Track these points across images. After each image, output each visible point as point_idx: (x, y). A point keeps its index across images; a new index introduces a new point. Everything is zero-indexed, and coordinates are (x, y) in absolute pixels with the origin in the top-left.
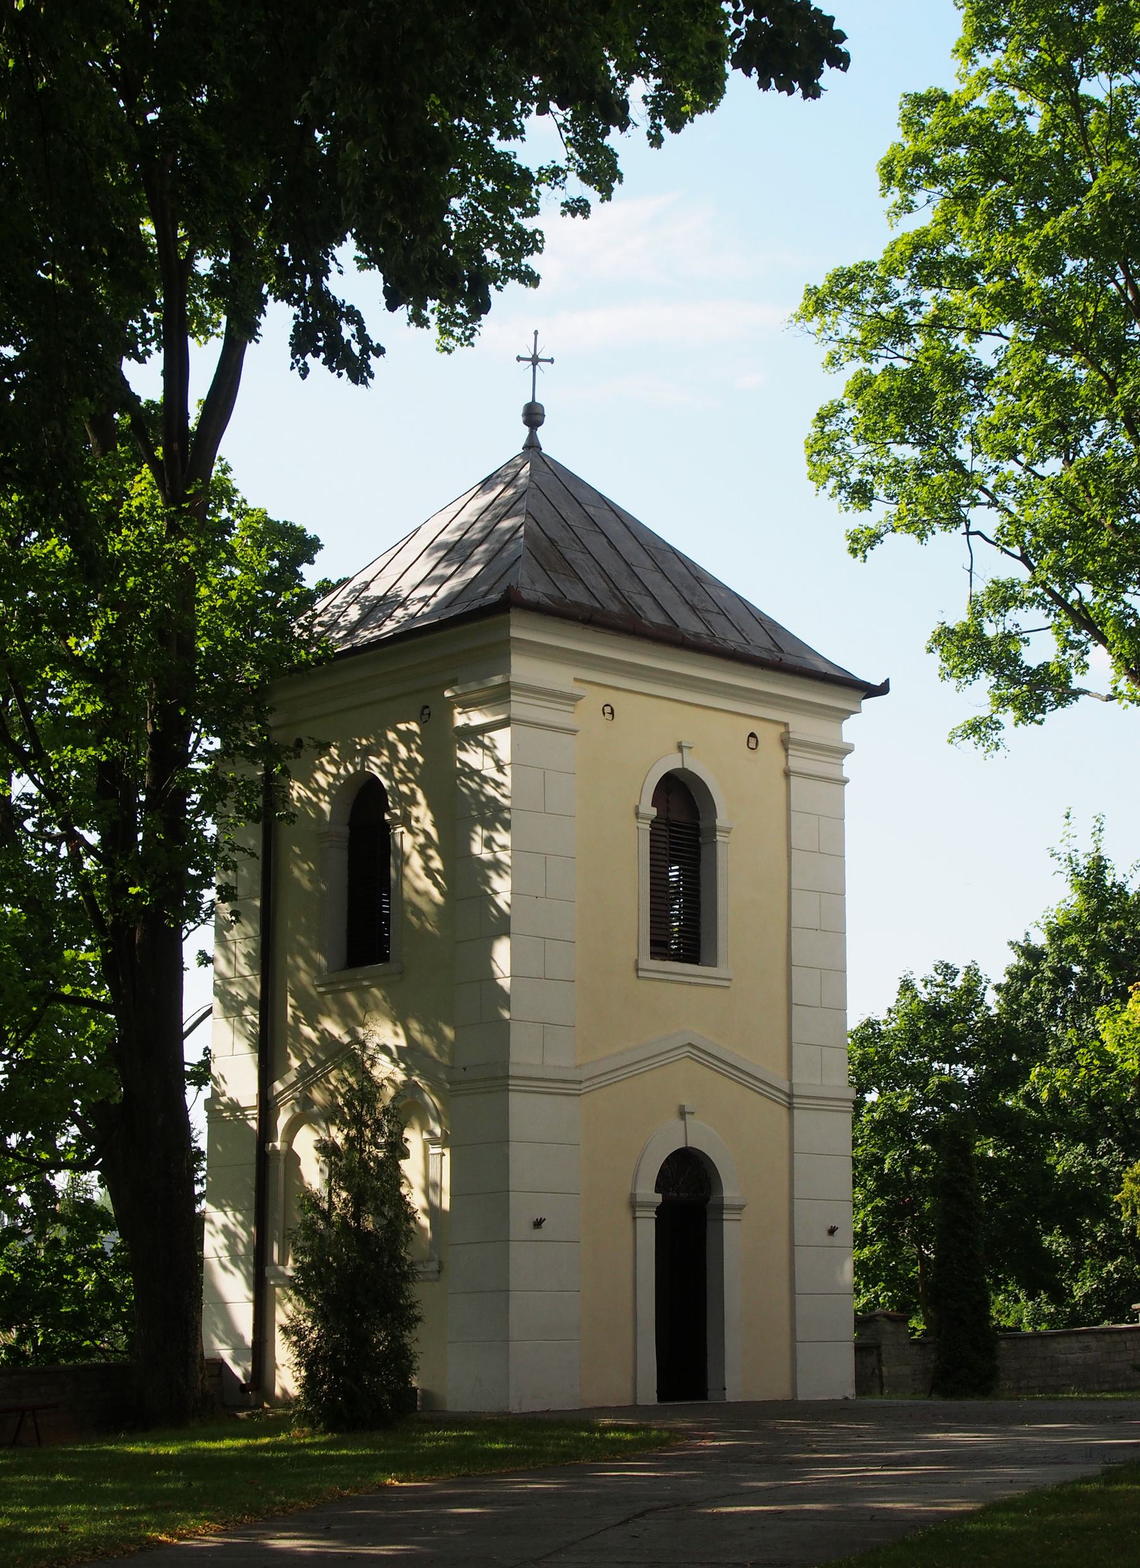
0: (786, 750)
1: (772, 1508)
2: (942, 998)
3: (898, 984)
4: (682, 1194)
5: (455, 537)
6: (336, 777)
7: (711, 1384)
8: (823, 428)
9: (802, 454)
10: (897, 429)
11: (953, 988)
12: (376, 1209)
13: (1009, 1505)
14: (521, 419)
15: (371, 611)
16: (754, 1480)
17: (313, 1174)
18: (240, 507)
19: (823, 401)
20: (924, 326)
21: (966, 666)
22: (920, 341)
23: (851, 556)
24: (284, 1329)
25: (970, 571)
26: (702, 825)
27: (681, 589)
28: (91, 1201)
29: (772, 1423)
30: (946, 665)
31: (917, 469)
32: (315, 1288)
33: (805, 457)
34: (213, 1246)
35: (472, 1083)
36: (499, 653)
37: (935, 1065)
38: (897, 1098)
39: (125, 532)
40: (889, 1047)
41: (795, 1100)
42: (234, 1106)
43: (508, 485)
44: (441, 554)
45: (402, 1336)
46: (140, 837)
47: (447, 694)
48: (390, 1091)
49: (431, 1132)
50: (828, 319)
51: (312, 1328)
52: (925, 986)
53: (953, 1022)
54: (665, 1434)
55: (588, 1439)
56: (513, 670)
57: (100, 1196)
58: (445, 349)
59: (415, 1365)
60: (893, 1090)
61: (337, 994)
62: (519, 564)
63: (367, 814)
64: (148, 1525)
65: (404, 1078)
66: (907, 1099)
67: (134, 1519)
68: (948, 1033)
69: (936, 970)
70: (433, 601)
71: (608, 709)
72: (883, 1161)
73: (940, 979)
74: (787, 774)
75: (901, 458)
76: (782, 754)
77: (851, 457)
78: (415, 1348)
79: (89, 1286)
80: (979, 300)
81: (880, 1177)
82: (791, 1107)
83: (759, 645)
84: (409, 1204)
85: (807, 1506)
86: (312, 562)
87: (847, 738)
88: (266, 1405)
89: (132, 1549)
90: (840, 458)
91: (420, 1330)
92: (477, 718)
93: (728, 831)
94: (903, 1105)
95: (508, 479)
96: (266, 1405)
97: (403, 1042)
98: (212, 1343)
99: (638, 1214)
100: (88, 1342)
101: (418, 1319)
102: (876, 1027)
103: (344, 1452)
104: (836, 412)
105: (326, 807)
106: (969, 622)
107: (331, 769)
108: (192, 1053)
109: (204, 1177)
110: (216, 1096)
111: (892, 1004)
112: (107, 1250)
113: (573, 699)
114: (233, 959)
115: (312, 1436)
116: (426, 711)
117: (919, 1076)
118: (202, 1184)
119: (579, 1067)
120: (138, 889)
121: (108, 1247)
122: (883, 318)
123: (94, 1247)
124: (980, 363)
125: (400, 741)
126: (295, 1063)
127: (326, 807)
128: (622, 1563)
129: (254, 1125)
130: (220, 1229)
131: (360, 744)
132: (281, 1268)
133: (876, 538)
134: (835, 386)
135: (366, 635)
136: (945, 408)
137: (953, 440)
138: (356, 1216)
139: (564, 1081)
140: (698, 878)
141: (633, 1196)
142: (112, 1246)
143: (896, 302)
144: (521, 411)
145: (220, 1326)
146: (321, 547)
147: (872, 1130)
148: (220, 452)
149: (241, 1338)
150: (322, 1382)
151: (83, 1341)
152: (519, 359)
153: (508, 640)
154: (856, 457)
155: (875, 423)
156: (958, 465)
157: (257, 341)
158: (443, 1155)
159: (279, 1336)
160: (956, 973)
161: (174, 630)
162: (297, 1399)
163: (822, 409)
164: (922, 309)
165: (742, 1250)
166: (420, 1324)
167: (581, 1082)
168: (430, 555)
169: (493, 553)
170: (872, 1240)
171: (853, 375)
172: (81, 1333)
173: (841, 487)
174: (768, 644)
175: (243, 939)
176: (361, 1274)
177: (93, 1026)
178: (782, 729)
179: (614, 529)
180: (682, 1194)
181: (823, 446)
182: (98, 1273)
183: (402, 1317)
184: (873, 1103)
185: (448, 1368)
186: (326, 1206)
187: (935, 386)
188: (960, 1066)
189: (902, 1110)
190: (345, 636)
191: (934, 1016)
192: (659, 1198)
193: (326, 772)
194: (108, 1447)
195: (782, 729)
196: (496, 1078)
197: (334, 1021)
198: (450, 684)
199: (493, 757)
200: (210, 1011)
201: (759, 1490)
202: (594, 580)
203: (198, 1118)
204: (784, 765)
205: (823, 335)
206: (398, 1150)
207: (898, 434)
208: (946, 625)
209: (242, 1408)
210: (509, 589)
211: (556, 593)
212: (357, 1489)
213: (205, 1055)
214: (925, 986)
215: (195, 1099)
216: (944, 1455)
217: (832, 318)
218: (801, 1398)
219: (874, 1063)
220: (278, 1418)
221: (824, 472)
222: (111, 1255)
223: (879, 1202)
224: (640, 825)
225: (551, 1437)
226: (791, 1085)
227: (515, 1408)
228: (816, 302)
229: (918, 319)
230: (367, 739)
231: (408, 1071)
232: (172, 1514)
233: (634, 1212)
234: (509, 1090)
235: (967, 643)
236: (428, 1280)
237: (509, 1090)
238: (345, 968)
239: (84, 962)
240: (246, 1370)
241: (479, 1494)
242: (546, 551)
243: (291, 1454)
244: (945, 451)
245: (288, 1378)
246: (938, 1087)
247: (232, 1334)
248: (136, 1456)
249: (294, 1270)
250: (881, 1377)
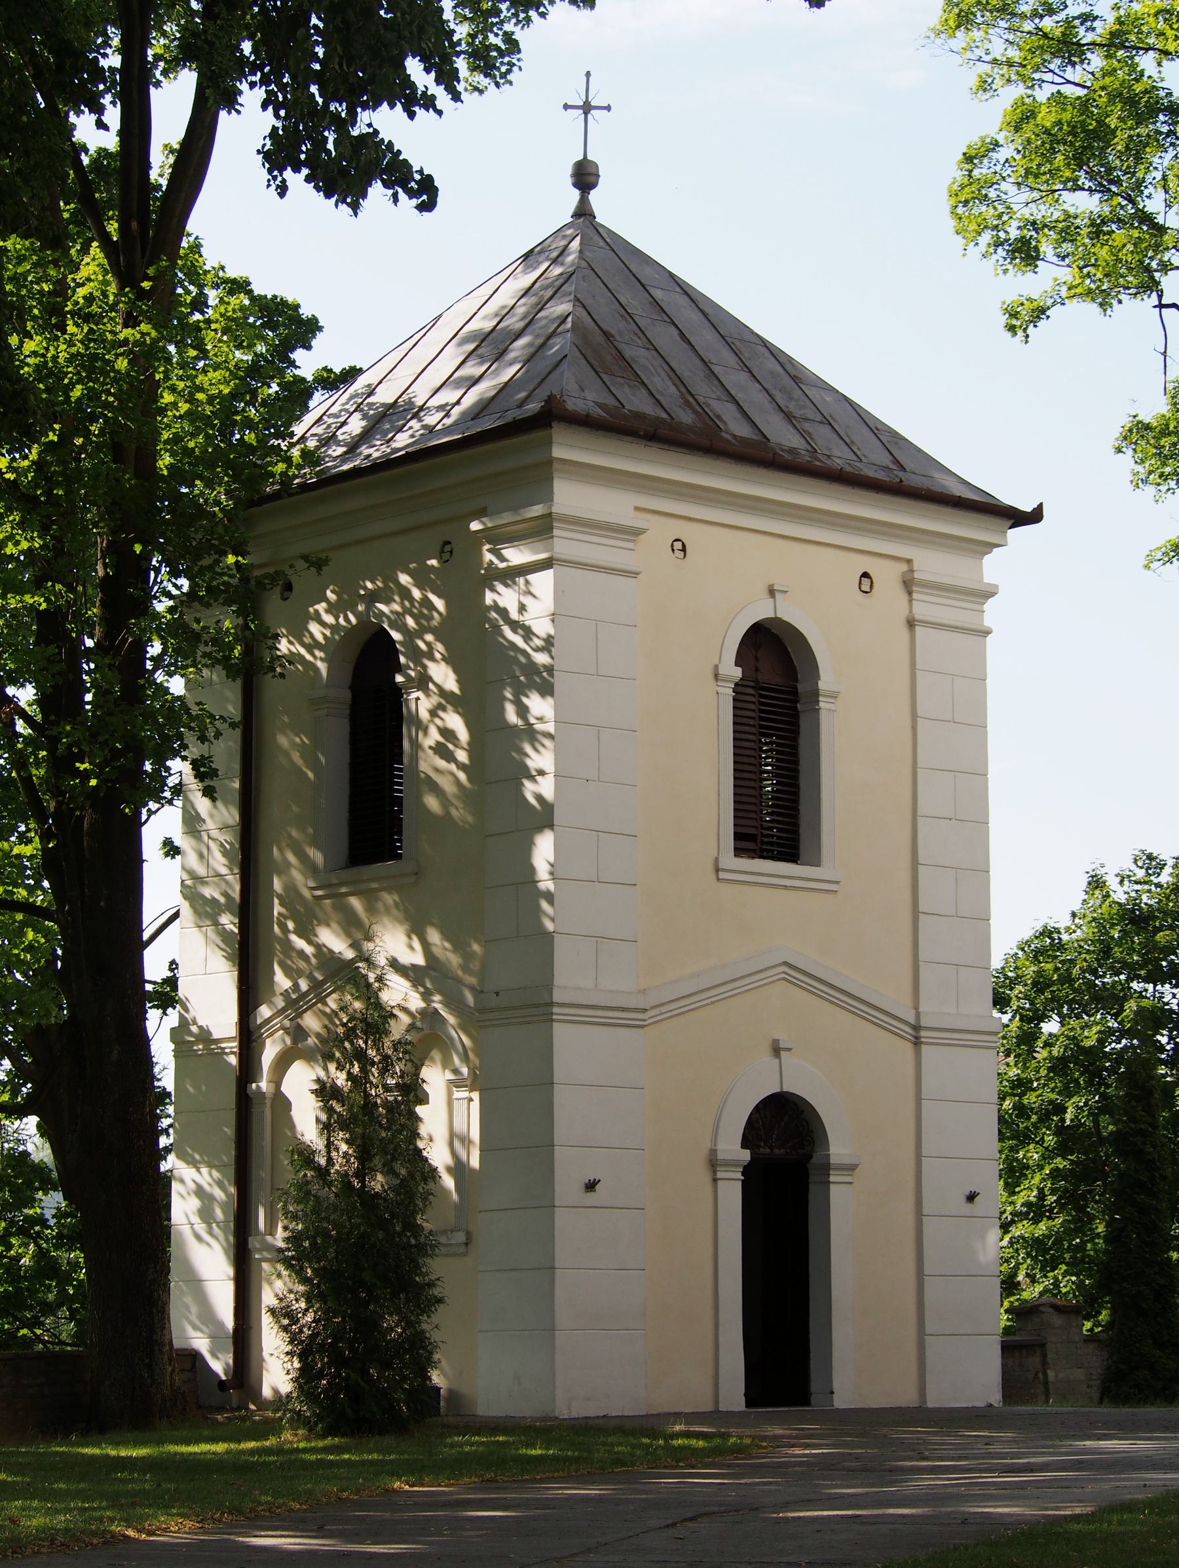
0: (910, 593)
1: (850, 1512)
2: (1144, 898)
3: (1083, 881)
4: (776, 1151)
5: (488, 325)
6: (335, 628)
7: (815, 1385)
8: (971, 171)
9: (945, 204)
10: (1068, 174)
11: (1158, 885)
12: (384, 1165)
13: (1130, 1507)
14: (569, 181)
15: (378, 422)
16: (841, 1487)
17: (306, 1118)
18: (217, 276)
19: (970, 137)
20: (1099, 45)
21: (1167, 470)
22: (1096, 61)
23: (1009, 334)
24: (272, 1311)
25: (1164, 354)
26: (801, 688)
27: (773, 392)
28: (26, 1154)
29: (885, 1430)
30: (1139, 468)
31: (1092, 225)
32: (310, 1262)
33: (947, 209)
34: (183, 1209)
35: (509, 1007)
36: (540, 477)
37: (1135, 985)
38: (1082, 1028)
39: (71, 329)
40: (1072, 962)
41: (923, 1033)
42: (205, 1036)
43: (555, 261)
44: (472, 346)
45: (419, 1323)
46: (88, 697)
47: (475, 526)
48: (405, 1019)
49: (456, 1071)
50: (977, 34)
51: (307, 1310)
52: (1121, 882)
53: (1158, 930)
54: (748, 1441)
55: (648, 1446)
56: (556, 499)
57: (39, 1150)
58: (476, 89)
59: (436, 1357)
60: (1078, 1017)
61: (339, 900)
62: (564, 365)
63: (373, 672)
64: (112, 1520)
65: (422, 1005)
66: (1095, 1029)
67: (97, 1514)
68: (1150, 946)
69: (1135, 861)
70: (456, 412)
71: (678, 545)
72: (1064, 1110)
73: (1140, 874)
74: (911, 624)
75: (1072, 211)
76: (904, 598)
77: (1008, 208)
78: (435, 1336)
79: (25, 1261)
80: (1165, 20)
81: (1060, 1130)
82: (917, 1042)
83: (874, 462)
84: (426, 1160)
85: (891, 1511)
86: (308, 347)
87: (987, 579)
88: (252, 1407)
89: (95, 1542)
90: (995, 208)
91: (441, 1315)
92: (516, 556)
93: (834, 696)
94: (1090, 1038)
95: (555, 254)
96: (252, 1407)
97: (419, 959)
98: (183, 1330)
99: (719, 1175)
100: (25, 1331)
101: (440, 1301)
102: (1055, 936)
103: (347, 1456)
104: (988, 151)
105: (322, 667)
106: (1168, 415)
107: (329, 619)
108: (154, 968)
109: (170, 1126)
110: (184, 1023)
111: (1076, 906)
112: (48, 1215)
113: (636, 532)
114: (205, 852)
115: (308, 1440)
116: (448, 548)
117: (1112, 1000)
118: (168, 1135)
119: (643, 992)
120: (86, 765)
121: (49, 1214)
122: (1045, 36)
123: (31, 1212)
124: (1170, 94)
125: (416, 585)
126: (282, 981)
127: (322, 667)
128: (658, 1562)
129: (233, 1060)
130: (192, 1191)
131: (365, 588)
132: (269, 1238)
133: (1040, 313)
134: (989, 117)
135: (375, 451)
136: (1127, 148)
137: (1139, 185)
138: (360, 1174)
139: (624, 1009)
140: (795, 755)
141: (713, 1152)
142: (54, 1211)
143: (1062, 16)
144: (569, 170)
145: (194, 1309)
146: (320, 329)
147: (1050, 1069)
148: (191, 226)
149: (221, 1325)
150: (320, 1375)
151: (18, 1329)
152: (566, 107)
153: (550, 462)
154: (1015, 207)
155: (1039, 166)
156: (1146, 218)
157: (238, 112)
158: (471, 1100)
159: (266, 1319)
160: (1162, 866)
161: (132, 447)
162: (289, 1396)
163: (969, 147)
164: (1096, 24)
165: (854, 1222)
166: (441, 1308)
168: (460, 344)
169: (532, 350)
170: (1051, 1211)
171: (1011, 102)
172: (16, 1319)
173: (998, 244)
174: (886, 460)
175: (218, 818)
176: (370, 1247)
177: (30, 935)
178: (904, 567)
179: (687, 316)
180: (776, 1151)
181: (971, 194)
182: (37, 1245)
183: (419, 1298)
184: (1050, 1035)
185: (473, 1362)
186: (323, 1161)
187: (1112, 122)
188: (1167, 986)
189: (1088, 1043)
190: (346, 453)
191: (1133, 921)
192: (746, 1155)
193: (323, 624)
194: (57, 1449)
195: (904, 567)
196: (537, 1006)
197: (333, 932)
198: (479, 514)
199: (532, 604)
200: (176, 915)
201: (842, 1496)
202: (660, 383)
203: (162, 1051)
204: (907, 612)
205: (969, 55)
206: (413, 1092)
207: (1068, 180)
208: (1139, 418)
209: (221, 1409)
210: (550, 399)
211: (612, 402)
212: (358, 1492)
213: (171, 970)
214: (1121, 882)
215: (159, 1027)
216: (1080, 1462)
217: (982, 33)
218: (930, 1405)
219: (1053, 983)
220: (266, 1421)
221: (973, 227)
222: (52, 1222)
223: (1060, 1163)
224: (720, 690)
225: (604, 1444)
226: (918, 1015)
227: (565, 1414)
228: (959, 15)
229: (1090, 38)
230: (373, 582)
231: (426, 996)
232: (139, 1510)
233: (715, 1172)
234: (552, 1020)
235: (1166, 442)
236: (455, 1255)
237: (552, 1020)
238: (347, 867)
239: (18, 856)
240: (227, 1364)
241: (505, 1499)
242: (600, 349)
243: (281, 1458)
244: (1132, 201)
245: (277, 1373)
246: (1136, 1013)
247: (208, 1315)
248: (93, 1457)
249: (287, 1240)
250: (1046, 1383)
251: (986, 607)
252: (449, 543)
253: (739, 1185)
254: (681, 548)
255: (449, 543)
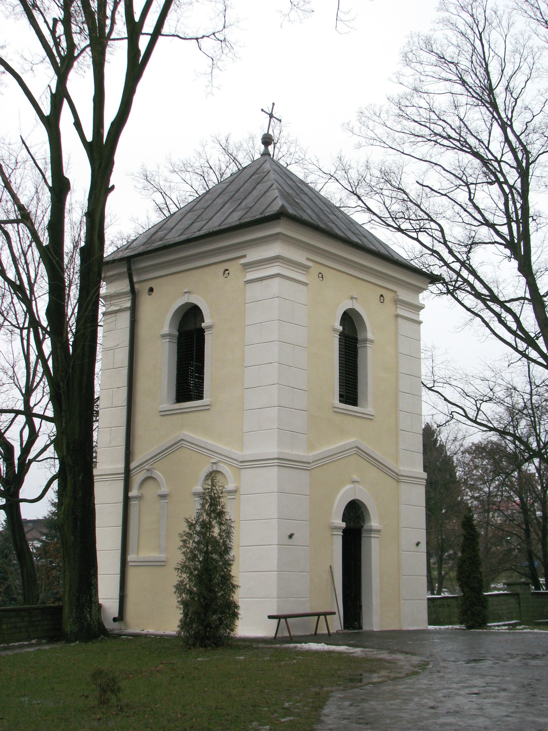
26: (360, 337)
71: (320, 275)
83: (383, 251)
87: (422, 302)
116: (227, 272)
167: (309, 463)
192: (344, 525)
251: (420, 313)
252: (227, 270)
253: (341, 538)
254: (321, 276)
255: (227, 270)
